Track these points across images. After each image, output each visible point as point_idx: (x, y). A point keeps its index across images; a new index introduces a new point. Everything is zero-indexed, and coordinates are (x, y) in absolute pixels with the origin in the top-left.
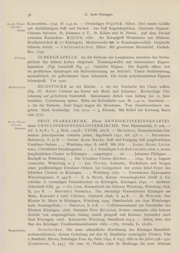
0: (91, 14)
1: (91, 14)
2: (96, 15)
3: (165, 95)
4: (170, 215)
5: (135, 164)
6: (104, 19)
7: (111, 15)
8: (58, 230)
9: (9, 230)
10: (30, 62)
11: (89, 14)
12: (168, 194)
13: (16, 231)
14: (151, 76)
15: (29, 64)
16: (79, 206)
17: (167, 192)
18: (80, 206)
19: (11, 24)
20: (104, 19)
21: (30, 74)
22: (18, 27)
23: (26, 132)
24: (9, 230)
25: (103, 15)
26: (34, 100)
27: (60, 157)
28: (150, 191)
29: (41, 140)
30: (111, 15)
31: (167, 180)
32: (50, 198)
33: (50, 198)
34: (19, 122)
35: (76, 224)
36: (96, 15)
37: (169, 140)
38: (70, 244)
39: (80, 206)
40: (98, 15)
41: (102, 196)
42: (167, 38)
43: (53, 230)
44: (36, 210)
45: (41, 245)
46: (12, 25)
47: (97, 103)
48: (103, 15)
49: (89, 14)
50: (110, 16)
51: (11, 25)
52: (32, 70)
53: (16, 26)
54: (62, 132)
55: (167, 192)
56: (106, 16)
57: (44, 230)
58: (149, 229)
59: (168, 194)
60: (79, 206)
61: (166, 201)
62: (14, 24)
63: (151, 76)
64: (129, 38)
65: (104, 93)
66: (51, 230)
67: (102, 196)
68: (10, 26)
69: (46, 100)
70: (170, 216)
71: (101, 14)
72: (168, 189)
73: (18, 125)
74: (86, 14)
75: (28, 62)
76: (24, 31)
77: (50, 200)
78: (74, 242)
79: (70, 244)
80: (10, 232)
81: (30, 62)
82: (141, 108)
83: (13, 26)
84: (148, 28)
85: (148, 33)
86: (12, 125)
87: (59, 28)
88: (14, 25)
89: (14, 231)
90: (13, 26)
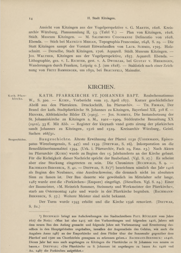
0: (94, 18)
1: (94, 18)
2: (98, 18)
3: (160, 219)
6: (108, 23)
7: (114, 18)
8: (66, 139)
9: (9, 139)
10: (32, 144)
11: (91, 18)
12: (171, 223)
13: (17, 140)
15: (30, 146)
17: (170, 221)
19: (11, 96)
20: (108, 23)
21: (31, 122)
24: (9, 139)
29: (43, 196)
30: (114, 18)
31: (171, 147)
35: (50, 149)
36: (98, 18)
40: (101, 18)
43: (61, 139)
46: (14, 97)
48: (105, 18)
49: (91, 18)
51: (12, 97)
52: (33, 118)
54: (66, 188)
55: (170, 221)
57: (52, 139)
58: (163, 51)
59: (171, 223)
62: (15, 96)
64: (126, 187)
66: (59, 139)
71: (103, 18)
72: (171, 219)
74: (89, 18)
75: (30, 144)
76: (25, 140)
80: (10, 141)
81: (32, 144)
83: (14, 97)
86: (13, 99)
87: (60, 124)
88: (15, 97)
89: (14, 140)
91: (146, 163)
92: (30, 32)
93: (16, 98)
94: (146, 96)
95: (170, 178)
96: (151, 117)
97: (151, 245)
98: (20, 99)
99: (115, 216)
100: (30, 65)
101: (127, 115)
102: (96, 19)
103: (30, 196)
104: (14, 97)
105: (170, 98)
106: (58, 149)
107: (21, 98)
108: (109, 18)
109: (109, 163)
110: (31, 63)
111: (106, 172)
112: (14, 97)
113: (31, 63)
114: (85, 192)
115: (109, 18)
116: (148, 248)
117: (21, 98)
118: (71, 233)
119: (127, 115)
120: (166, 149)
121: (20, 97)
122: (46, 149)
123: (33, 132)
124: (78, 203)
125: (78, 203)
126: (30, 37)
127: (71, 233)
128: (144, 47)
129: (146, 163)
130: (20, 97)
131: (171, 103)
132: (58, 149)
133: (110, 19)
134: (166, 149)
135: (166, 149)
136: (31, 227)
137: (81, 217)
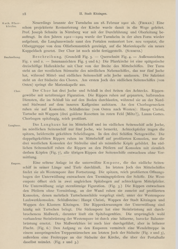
0: (86, 14)
1: (86, 14)
2: (90, 14)
4: (163, 148)
7: (106, 14)
12: (161, 132)
14: (126, 139)
19: (5, 24)
25: (97, 14)
28: (143, 200)
30: (106, 14)
33: (123, 64)
34: (13, 24)
36: (90, 14)
37: (163, 105)
40: (93, 14)
42: (122, 177)
44: (55, 205)
45: (134, 52)
46: (7, 25)
47: (111, 77)
48: (97, 14)
49: (83, 13)
51: (6, 25)
53: (11, 25)
56: (100, 15)
61: (160, 148)
62: (9, 23)
63: (126, 139)
68: (5, 25)
70: (164, 149)
74: (81, 14)
77: (123, 65)
82: (104, 235)
83: (7, 25)
84: (130, 46)
86: (7, 27)
92: (23, 28)
93: (9, 25)
95: (161, 173)
97: (139, 236)
98: (13, 26)
99: (89, 13)
100: (25, 205)
101: (137, 51)
102: (88, 14)
103: (25, 242)
104: (7, 25)
105: (161, 93)
106: (59, 62)
107: (14, 25)
108: (100, 14)
110: (25, 202)
112: (7, 25)
113: (25, 202)
115: (100, 14)
117: (14, 25)
119: (137, 51)
121: (14, 25)
123: (27, 154)
126: (24, 139)
128: (133, 51)
130: (14, 25)
132: (59, 62)
133: (102, 14)
136: (25, 107)
137: (65, 229)
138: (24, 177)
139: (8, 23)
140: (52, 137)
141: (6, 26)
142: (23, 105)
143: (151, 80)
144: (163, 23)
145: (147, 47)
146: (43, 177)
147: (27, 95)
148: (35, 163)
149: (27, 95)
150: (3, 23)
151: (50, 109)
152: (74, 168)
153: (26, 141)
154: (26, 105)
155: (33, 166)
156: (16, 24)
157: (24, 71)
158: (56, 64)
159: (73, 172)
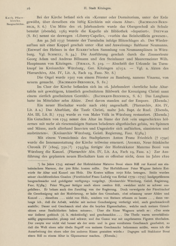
0: (90, 8)
1: (90, 8)
2: (95, 8)
5: (83, 73)
6: (102, 13)
7: (110, 8)
11: (88, 8)
16: (163, 31)
18: (164, 32)
19: (9, 18)
20: (102, 13)
22: (15, 21)
23: (24, 28)
25: (101, 8)
26: (146, 63)
27: (85, 132)
30: (110, 8)
32: (60, 24)
36: (95, 8)
38: (45, 77)
39: (164, 32)
40: (97, 8)
41: (85, 73)
48: (101, 8)
49: (88, 8)
50: (108, 10)
60: (163, 31)
62: (12, 18)
65: (38, 130)
67: (85, 73)
69: (50, 26)
71: (100, 8)
73: (17, 21)
74: (85, 8)
78: (108, 71)
79: (45, 77)
85: (98, 59)
86: (11, 21)
88: (12, 19)
90: (12, 19)
91: (34, 50)
93: (14, 20)
94: (108, 133)
96: (98, 94)
99: (93, 7)
102: (93, 9)
108: (104, 8)
109: (82, 54)
111: (103, 142)
114: (32, 129)
115: (104, 8)
116: (158, 70)
118: (33, 223)
120: (153, 68)
122: (118, 59)
124: (66, 120)
125: (66, 120)
127: (33, 223)
129: (34, 50)
131: (166, 66)
134: (153, 69)
135: (153, 69)
137: (31, 233)
138: (29, 202)
139: (11, 18)
140: (56, 104)
141: (10, 21)
142: (28, 129)
143: (113, 236)
144: (167, 18)
145: (124, 164)
146: (52, 27)
147: (31, 22)
148: (40, 105)
149: (31, 22)
150: (6, 18)
151: (58, 45)
152: (89, 41)
153: (31, 183)
154: (30, 129)
155: (37, 90)
156: (19, 18)
157: (29, 211)
158: (53, 213)
159: (72, 190)
